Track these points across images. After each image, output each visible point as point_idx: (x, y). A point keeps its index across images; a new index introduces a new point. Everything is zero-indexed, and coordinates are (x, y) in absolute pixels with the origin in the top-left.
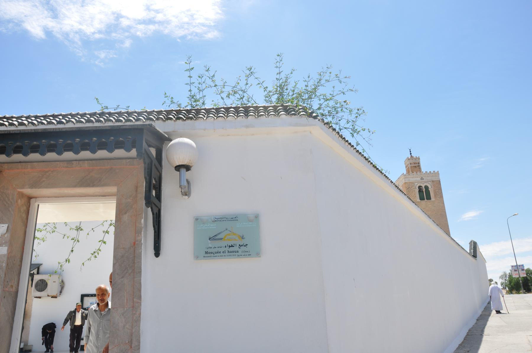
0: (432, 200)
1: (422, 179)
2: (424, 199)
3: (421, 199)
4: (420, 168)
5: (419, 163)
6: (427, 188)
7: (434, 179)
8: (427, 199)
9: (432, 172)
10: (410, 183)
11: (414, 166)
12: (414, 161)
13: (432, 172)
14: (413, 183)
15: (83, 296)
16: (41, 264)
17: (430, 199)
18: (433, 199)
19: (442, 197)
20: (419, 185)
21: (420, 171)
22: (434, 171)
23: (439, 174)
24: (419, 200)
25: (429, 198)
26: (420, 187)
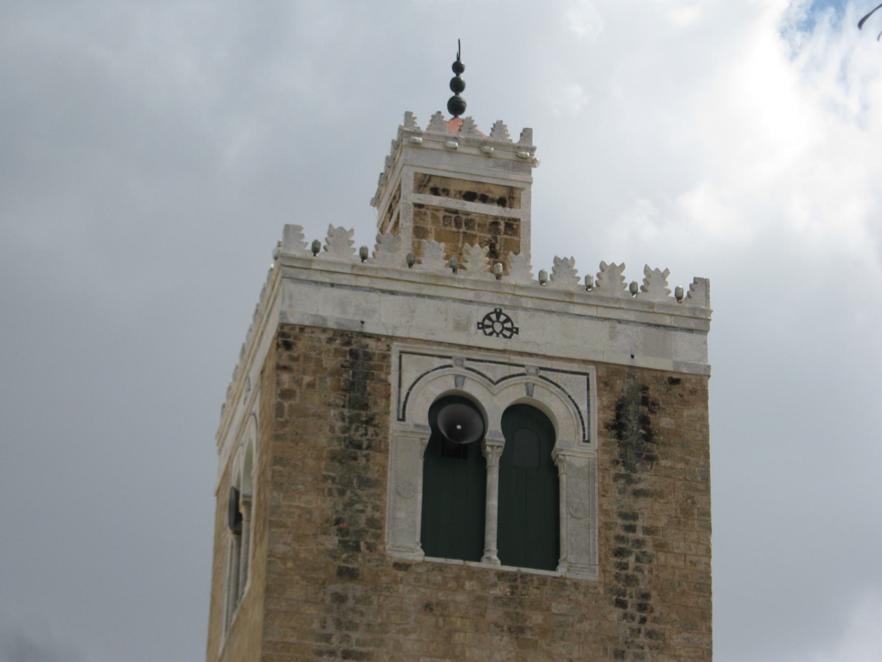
15: (401, 352)
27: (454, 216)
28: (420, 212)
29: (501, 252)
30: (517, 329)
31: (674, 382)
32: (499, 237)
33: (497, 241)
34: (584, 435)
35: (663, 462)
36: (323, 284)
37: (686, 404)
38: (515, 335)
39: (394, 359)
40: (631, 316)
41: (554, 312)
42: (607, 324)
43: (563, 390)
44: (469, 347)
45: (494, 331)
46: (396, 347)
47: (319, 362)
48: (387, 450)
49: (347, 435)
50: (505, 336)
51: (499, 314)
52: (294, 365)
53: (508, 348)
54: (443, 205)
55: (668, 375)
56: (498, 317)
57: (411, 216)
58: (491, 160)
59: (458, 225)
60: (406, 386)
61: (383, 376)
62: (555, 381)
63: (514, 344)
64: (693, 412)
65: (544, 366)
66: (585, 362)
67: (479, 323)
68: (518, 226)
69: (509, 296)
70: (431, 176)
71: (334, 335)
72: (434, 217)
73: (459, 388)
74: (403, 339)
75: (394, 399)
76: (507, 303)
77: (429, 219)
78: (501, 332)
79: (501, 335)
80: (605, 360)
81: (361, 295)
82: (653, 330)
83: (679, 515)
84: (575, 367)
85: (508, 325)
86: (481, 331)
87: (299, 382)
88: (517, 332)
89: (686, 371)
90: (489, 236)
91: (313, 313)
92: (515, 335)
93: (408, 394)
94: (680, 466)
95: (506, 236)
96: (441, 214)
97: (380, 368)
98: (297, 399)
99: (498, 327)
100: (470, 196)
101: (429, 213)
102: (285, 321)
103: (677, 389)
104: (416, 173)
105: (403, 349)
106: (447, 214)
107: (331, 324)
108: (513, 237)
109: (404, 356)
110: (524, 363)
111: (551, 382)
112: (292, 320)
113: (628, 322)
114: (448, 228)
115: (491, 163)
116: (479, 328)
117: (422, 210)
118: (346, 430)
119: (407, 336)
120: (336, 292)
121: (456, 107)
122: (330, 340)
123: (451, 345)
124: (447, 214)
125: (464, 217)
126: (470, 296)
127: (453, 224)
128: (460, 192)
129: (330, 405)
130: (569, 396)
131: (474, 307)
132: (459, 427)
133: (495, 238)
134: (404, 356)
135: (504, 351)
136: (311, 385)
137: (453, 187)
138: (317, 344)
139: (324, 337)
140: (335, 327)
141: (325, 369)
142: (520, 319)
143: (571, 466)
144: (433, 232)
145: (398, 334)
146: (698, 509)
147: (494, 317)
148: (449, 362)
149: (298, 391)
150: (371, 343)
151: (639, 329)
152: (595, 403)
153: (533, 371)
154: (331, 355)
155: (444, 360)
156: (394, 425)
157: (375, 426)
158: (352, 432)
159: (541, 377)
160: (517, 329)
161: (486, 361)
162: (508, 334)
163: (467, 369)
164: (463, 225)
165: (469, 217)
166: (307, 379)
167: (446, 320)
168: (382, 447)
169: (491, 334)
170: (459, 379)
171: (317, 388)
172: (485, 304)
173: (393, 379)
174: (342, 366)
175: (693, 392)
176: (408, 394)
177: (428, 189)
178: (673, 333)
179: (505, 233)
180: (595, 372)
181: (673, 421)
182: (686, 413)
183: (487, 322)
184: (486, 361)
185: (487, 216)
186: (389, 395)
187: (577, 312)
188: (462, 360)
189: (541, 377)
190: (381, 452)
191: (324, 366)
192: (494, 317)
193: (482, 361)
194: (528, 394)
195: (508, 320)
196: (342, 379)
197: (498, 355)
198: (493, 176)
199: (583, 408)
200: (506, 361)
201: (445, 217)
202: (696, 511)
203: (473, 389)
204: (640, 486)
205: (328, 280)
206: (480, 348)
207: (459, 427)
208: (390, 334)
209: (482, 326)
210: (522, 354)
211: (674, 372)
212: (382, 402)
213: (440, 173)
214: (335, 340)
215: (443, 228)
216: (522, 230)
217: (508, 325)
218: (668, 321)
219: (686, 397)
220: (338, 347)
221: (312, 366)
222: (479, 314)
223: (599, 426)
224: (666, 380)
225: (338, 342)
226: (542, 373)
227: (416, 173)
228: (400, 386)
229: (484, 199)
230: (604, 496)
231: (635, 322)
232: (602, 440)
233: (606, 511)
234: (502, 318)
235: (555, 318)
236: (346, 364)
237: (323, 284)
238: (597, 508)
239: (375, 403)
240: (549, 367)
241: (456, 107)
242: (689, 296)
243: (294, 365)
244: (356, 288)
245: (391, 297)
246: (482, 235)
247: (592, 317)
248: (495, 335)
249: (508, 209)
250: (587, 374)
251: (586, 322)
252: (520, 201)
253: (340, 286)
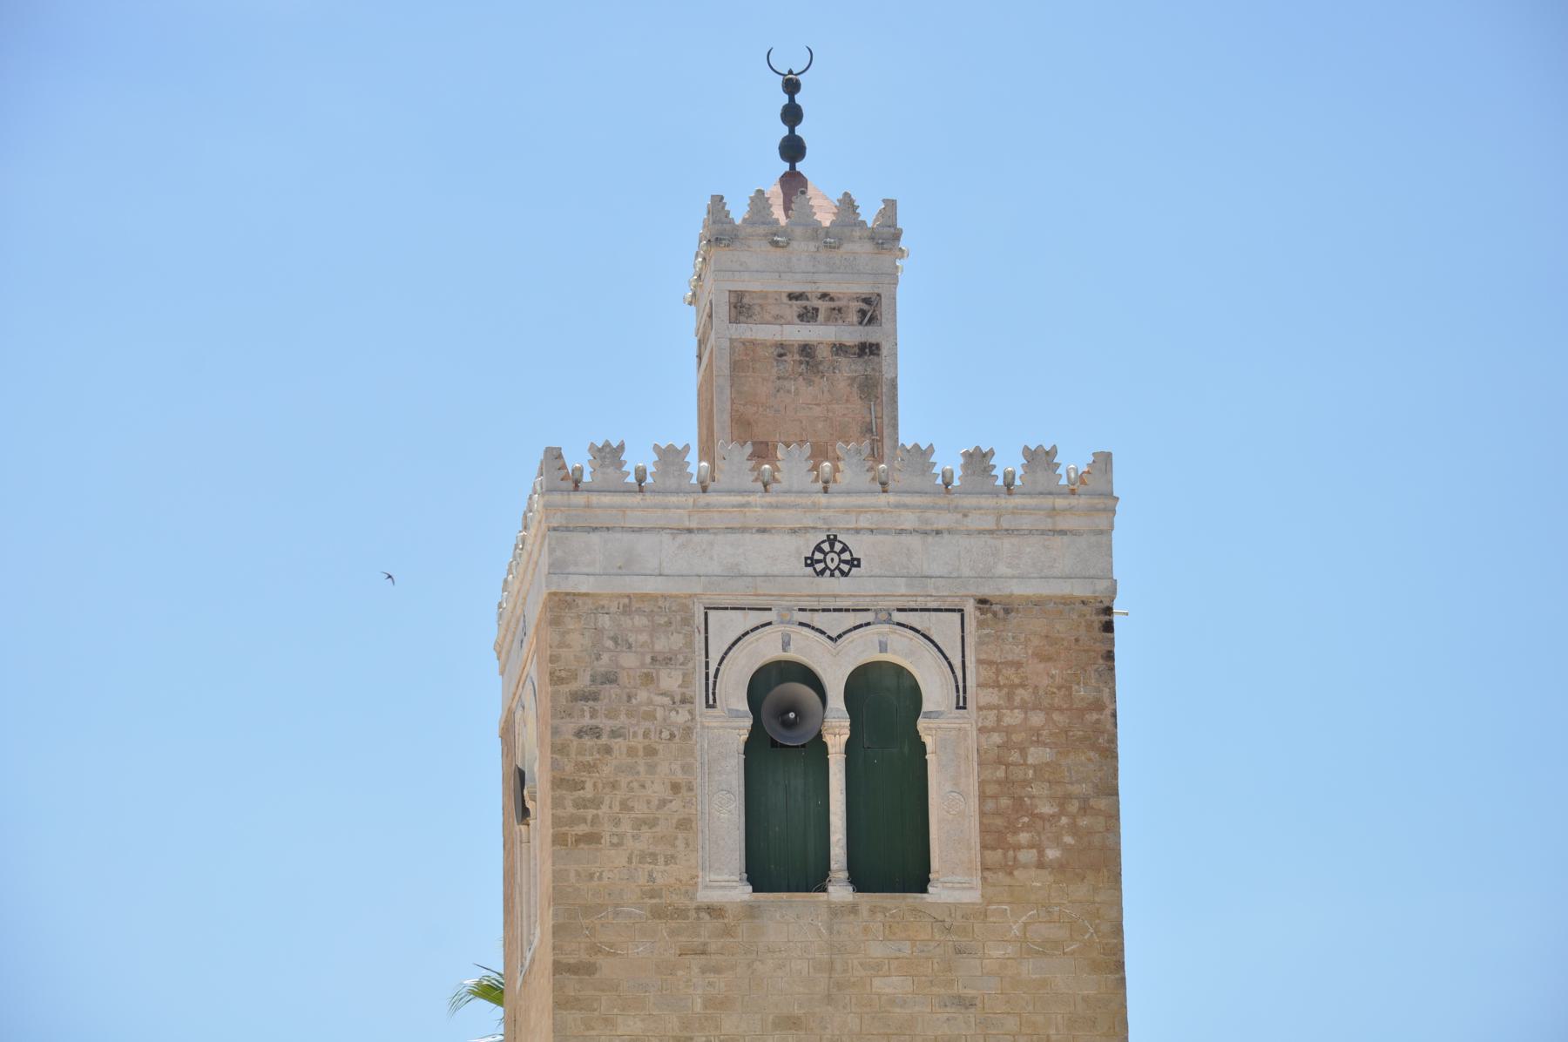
0: (938, 893)
1: (832, 557)
2: (816, 881)
3: (761, 874)
4: (876, 391)
5: (871, 310)
6: (884, 700)
7: (1023, 571)
8: (861, 881)
9: (1008, 461)
10: (629, 604)
11: (806, 338)
12: (804, 270)
13: (1008, 461)
14: (679, 614)
15: (961, 611)
16: (1026, 448)
17: (916, 878)
18: (955, 877)
19: (1100, 860)
20: (766, 649)
21: (876, 431)
22: (1041, 459)
23: (1106, 502)
24: (726, 883)
25: (894, 859)
26: (779, 694)
45: (827, 567)
51: (832, 541)
56: (832, 546)
85: (846, 556)
93: (718, 670)
109: (711, 614)
121: (793, 183)
132: (792, 715)
134: (957, 616)
147: (826, 547)
169: (822, 573)
176: (718, 670)
183: (818, 556)
188: (790, 609)
192: (826, 547)
195: (845, 549)
217: (846, 556)
222: (806, 545)
234: (838, 547)
241: (793, 183)
242: (801, 442)
250: (961, 611)
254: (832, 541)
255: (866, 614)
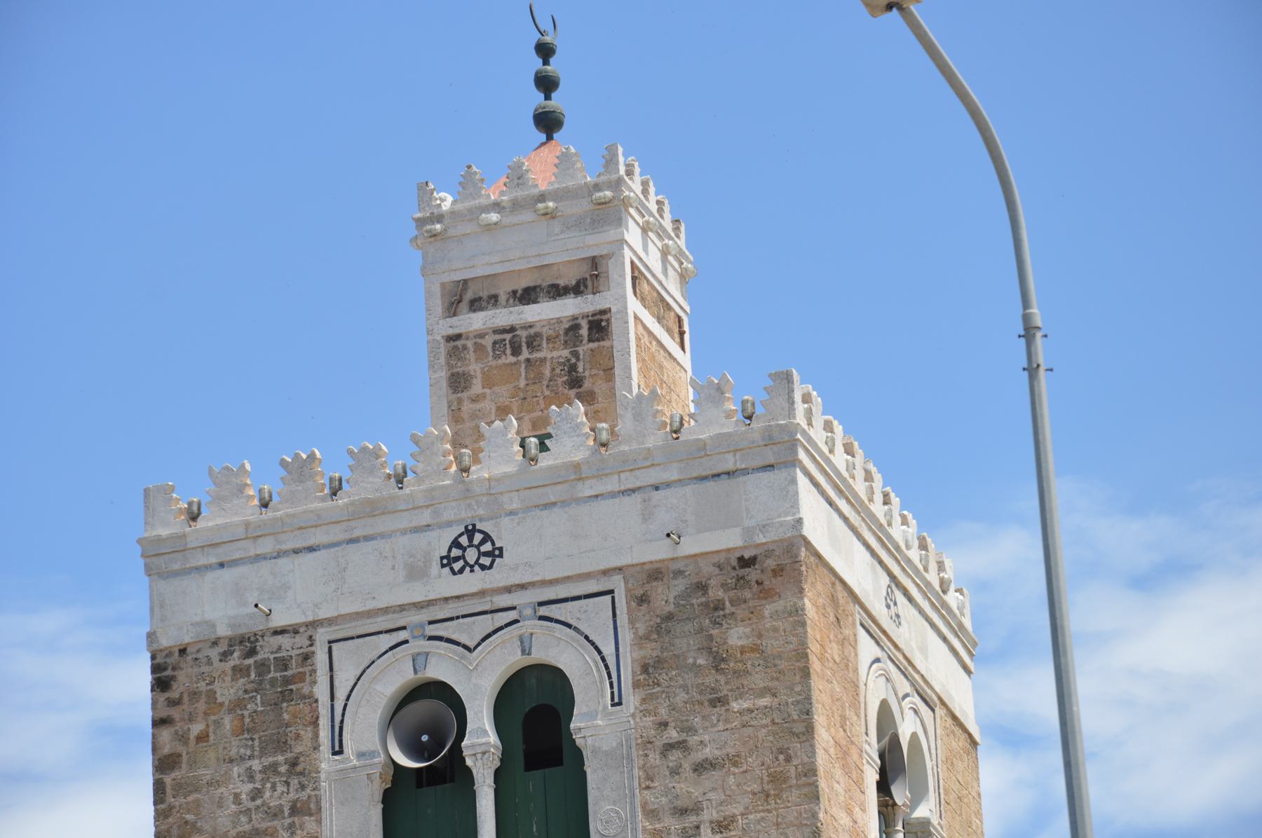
15: (330, 642)
26: (428, 713)
27: (508, 337)
28: (456, 347)
29: (587, 374)
30: (501, 549)
31: (745, 563)
32: (580, 350)
33: (578, 359)
34: (612, 693)
35: (735, 706)
36: (208, 568)
37: (766, 594)
38: (498, 560)
39: (321, 658)
40: (673, 475)
41: (554, 504)
42: (637, 497)
43: (576, 629)
44: (431, 603)
45: (466, 563)
46: (322, 636)
47: (211, 695)
48: (320, 809)
49: (259, 802)
50: (483, 567)
52: (175, 713)
53: (488, 586)
54: (489, 325)
55: (738, 555)
56: (471, 539)
57: (442, 360)
58: (556, 222)
59: (516, 351)
60: (341, 694)
61: (306, 690)
62: (562, 619)
63: (499, 576)
64: (778, 605)
65: (545, 599)
66: (605, 572)
67: (442, 558)
68: (608, 321)
69: (485, 499)
70: (465, 282)
71: (231, 646)
72: (479, 348)
73: (420, 675)
74: (330, 621)
75: (324, 722)
76: (481, 512)
77: (471, 356)
78: (477, 562)
79: (477, 568)
80: (635, 561)
81: (265, 567)
82: (710, 484)
83: (766, 787)
84: (593, 587)
86: (447, 569)
87: (183, 738)
88: (501, 556)
89: (764, 541)
90: (566, 353)
91: (198, 619)
92: (498, 560)
94: (765, 701)
95: (592, 345)
96: (488, 341)
97: (300, 677)
98: (184, 766)
99: (471, 555)
100: (528, 296)
101: (470, 344)
102: (155, 646)
103: (752, 574)
104: (443, 285)
105: (333, 637)
106: (498, 337)
107: (223, 631)
108: (602, 343)
109: (609, 598)
110: (515, 604)
111: (557, 621)
112: (165, 642)
113: (668, 485)
114: (503, 360)
115: (556, 226)
116: (443, 566)
117: (459, 343)
118: (256, 794)
119: (336, 614)
120: (228, 574)
122: (225, 656)
123: (402, 608)
124: (498, 337)
125: (523, 334)
126: (425, 517)
127: (508, 351)
128: (515, 292)
129: (231, 761)
130: (587, 638)
131: (432, 535)
132: (425, 738)
133: (575, 354)
134: (334, 646)
135: (482, 593)
136: (202, 738)
137: (503, 291)
138: (205, 669)
139: (214, 653)
140: (229, 633)
141: (221, 704)
142: (504, 534)
143: (595, 751)
144: (479, 375)
145: (323, 614)
146: (796, 766)
147: (464, 541)
148: (402, 635)
149: (184, 754)
150: (285, 641)
151: (688, 490)
152: (626, 636)
153: (528, 612)
154: (228, 679)
155: (395, 634)
156: (326, 763)
157: (302, 774)
158: (267, 794)
159: (542, 618)
160: (501, 549)
161: (458, 618)
162: (486, 561)
163: (431, 638)
164: (524, 348)
165: (532, 331)
166: (196, 729)
167: (393, 568)
168: (312, 806)
169: (461, 571)
170: (418, 660)
171: (212, 737)
172: (449, 524)
173: (321, 691)
174: (246, 691)
175: (778, 571)
177: (464, 306)
178: (741, 479)
179: (590, 340)
180: (622, 584)
181: (748, 630)
182: (768, 609)
183: (456, 552)
184: (458, 618)
185: (559, 321)
186: (317, 718)
187: (588, 493)
188: (422, 626)
189: (542, 618)
190: (311, 815)
191: (220, 700)
193: (451, 619)
194: (523, 652)
195: (487, 538)
196: (246, 713)
197: (475, 601)
198: (562, 251)
199: (608, 650)
200: (487, 607)
201: (495, 343)
202: (793, 770)
203: (438, 670)
204: (708, 752)
205: (213, 560)
206: (446, 599)
207: (425, 738)
208: (310, 619)
209: (447, 561)
210: (508, 590)
211: (745, 548)
212: (306, 734)
213: (479, 272)
214: (232, 653)
215: (494, 363)
216: (615, 327)
217: (487, 547)
218: (730, 463)
219: (767, 583)
220: (238, 662)
221: (201, 706)
222: (441, 543)
223: (634, 672)
224: (735, 563)
225: (236, 654)
226: (543, 611)
227: (443, 285)
228: (332, 698)
229: (557, 292)
230: (648, 788)
231: (680, 480)
232: (641, 693)
233: (653, 811)
235: (557, 514)
236: (249, 687)
237: (208, 568)
238: (639, 810)
239: (298, 736)
240: (553, 597)
243: (175, 713)
244: (258, 558)
245: (310, 557)
246: (555, 354)
247: (613, 495)
248: (468, 569)
249: (590, 297)
251: (605, 505)
252: (608, 277)
253: (234, 563)
254: (470, 532)
255: (500, 615)
